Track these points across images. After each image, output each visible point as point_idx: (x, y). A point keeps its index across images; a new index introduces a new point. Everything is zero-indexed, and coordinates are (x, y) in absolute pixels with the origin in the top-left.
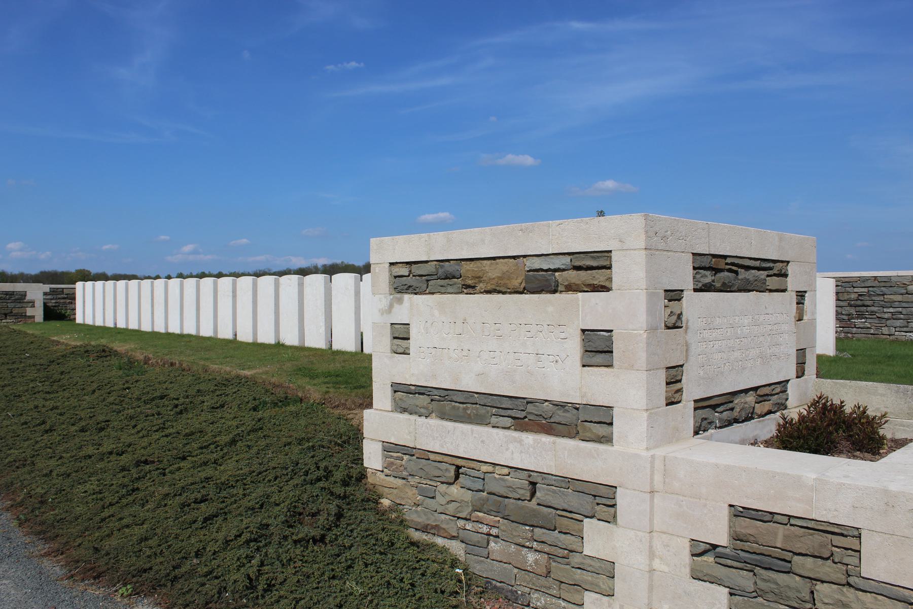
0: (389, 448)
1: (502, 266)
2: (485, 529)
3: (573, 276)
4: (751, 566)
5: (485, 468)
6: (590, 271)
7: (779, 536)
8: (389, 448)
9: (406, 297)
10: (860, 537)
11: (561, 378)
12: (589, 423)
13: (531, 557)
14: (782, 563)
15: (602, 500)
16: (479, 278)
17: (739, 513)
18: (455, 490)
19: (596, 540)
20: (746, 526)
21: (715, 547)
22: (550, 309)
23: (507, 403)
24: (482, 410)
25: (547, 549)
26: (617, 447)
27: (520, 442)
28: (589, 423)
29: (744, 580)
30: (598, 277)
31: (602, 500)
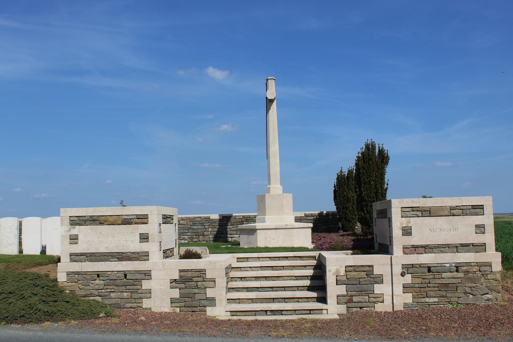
0: (68, 274)
1: (114, 218)
2: (109, 290)
3: (137, 220)
4: (183, 283)
5: (109, 273)
6: (143, 219)
7: (189, 274)
8: (68, 274)
9: (77, 227)
10: (483, 209)
11: (134, 245)
12: (143, 256)
13: (125, 294)
14: (190, 280)
15: (147, 275)
16: (106, 221)
17: (180, 271)
18: (97, 282)
19: (146, 285)
20: (183, 274)
21: (175, 280)
22: (130, 229)
23: (116, 254)
24: (107, 257)
25: (131, 291)
26: (151, 260)
27: (122, 264)
28: (143, 256)
29: (183, 286)
30: (145, 221)
31: (147, 275)
